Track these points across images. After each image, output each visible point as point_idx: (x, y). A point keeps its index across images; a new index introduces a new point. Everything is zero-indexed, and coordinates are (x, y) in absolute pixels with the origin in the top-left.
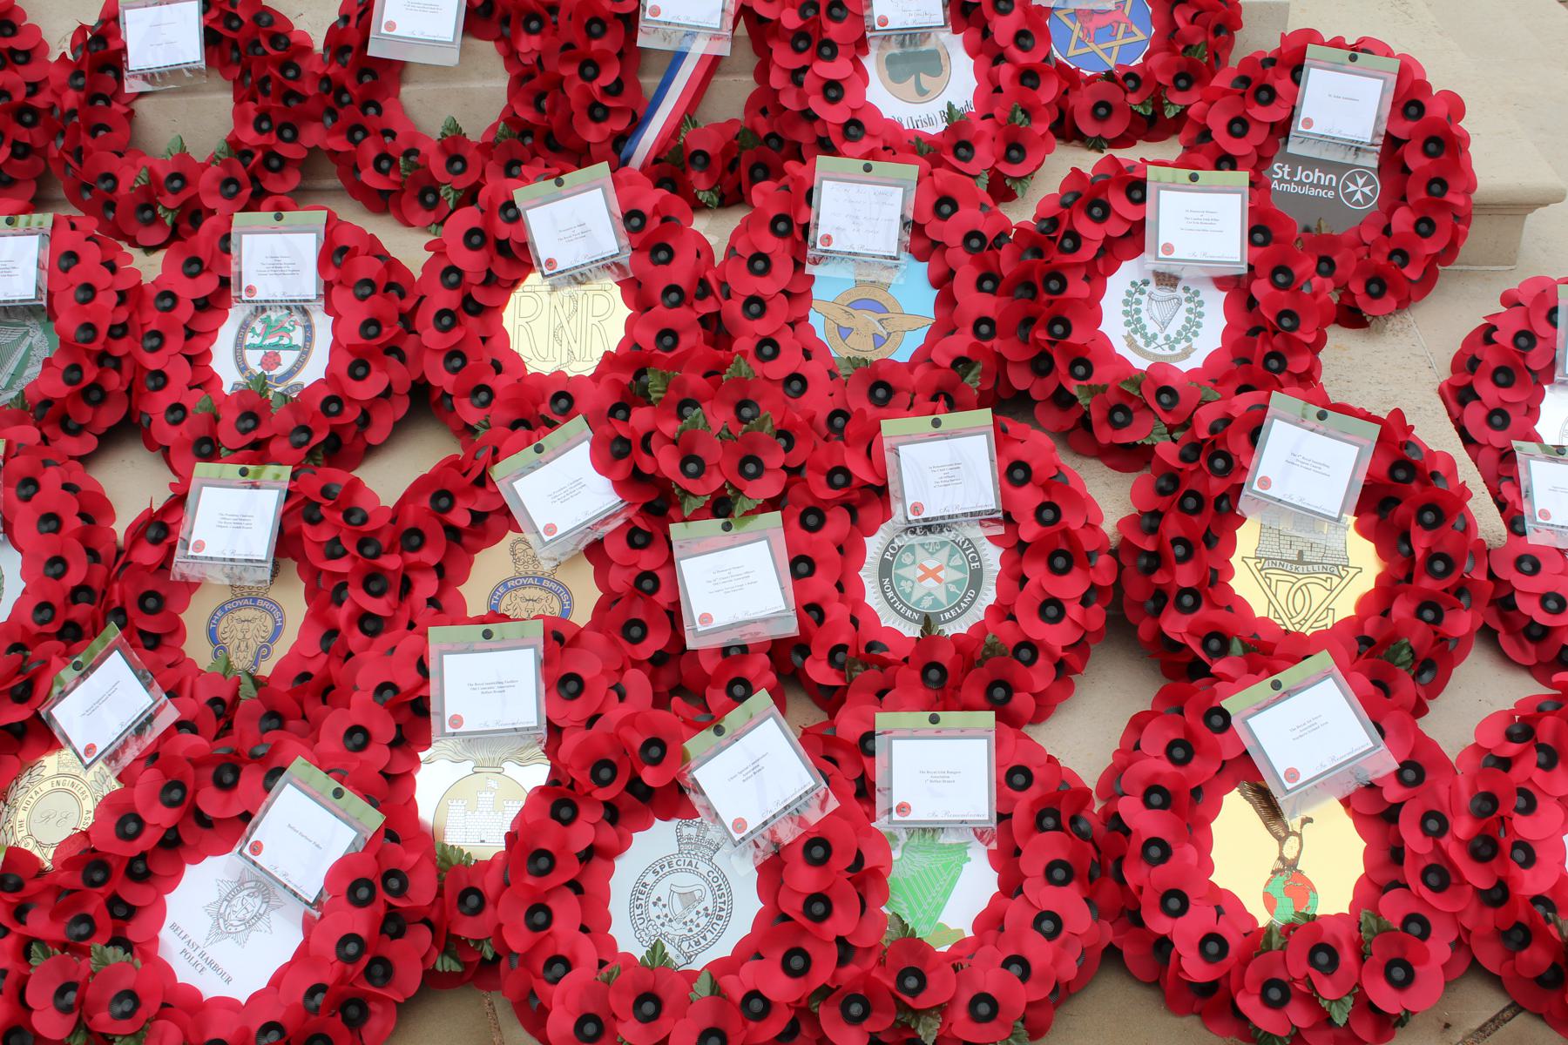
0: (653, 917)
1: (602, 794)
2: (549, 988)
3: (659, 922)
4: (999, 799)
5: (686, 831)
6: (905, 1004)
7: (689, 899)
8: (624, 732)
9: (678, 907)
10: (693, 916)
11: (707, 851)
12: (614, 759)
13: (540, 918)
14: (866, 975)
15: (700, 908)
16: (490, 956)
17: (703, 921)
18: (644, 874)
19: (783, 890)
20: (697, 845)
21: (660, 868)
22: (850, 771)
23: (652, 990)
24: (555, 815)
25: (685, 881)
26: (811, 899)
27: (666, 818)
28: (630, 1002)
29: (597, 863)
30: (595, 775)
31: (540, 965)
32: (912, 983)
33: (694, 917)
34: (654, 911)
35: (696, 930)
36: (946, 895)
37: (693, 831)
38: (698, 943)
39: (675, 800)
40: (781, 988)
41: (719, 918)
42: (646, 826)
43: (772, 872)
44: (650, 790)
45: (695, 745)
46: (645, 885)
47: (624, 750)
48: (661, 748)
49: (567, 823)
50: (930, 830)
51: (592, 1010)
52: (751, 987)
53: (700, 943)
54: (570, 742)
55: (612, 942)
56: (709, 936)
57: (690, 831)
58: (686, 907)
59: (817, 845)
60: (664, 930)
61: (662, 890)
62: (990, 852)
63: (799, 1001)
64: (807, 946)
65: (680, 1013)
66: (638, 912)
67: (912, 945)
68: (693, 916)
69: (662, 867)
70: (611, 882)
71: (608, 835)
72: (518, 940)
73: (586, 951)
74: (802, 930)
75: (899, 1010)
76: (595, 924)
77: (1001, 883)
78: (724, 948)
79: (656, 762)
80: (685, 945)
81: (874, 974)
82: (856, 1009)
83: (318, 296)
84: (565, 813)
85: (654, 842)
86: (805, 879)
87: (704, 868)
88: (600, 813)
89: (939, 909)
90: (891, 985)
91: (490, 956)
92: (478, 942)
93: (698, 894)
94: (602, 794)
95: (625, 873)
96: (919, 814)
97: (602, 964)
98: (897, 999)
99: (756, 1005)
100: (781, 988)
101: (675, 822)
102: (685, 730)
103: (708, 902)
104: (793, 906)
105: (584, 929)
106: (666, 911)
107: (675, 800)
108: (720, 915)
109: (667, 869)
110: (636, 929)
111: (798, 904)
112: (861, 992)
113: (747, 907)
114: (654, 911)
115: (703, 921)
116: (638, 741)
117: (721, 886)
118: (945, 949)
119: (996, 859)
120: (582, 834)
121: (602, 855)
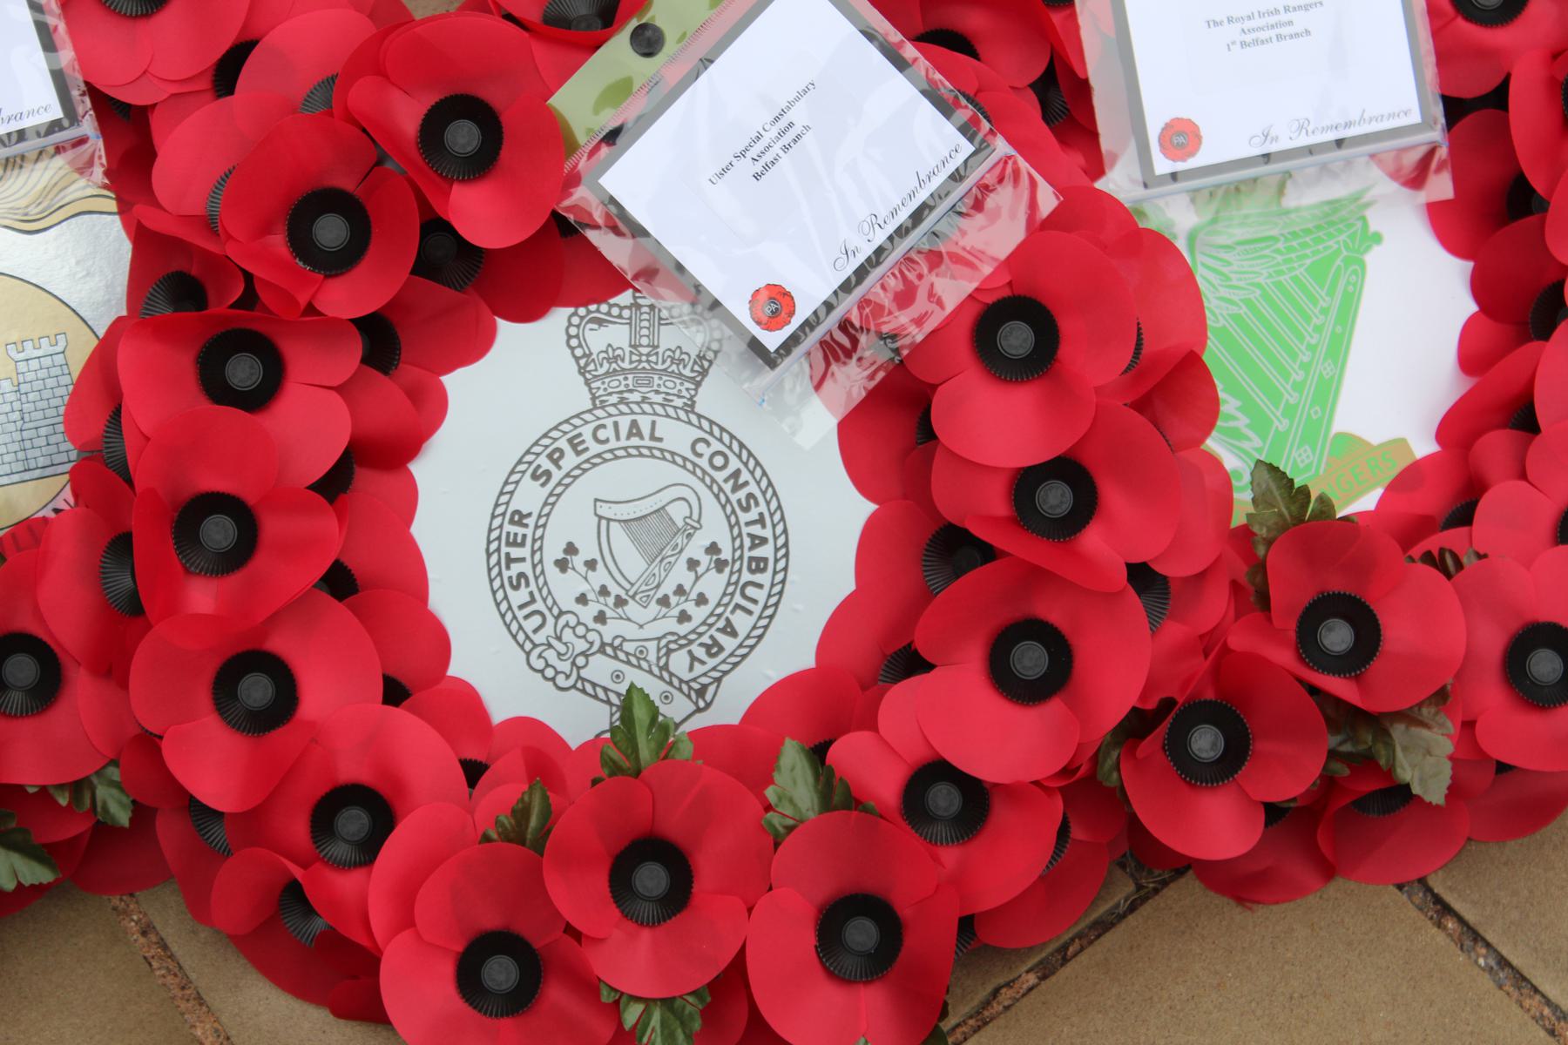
0: (568, 602)
1: (346, 298)
2: (347, 884)
3: (587, 613)
4: (1444, 57)
5: (598, 339)
6: (1338, 702)
7: (657, 531)
8: (362, 95)
9: (632, 563)
10: (680, 574)
11: (673, 385)
12: (346, 182)
13: (256, 690)
14: (1209, 642)
15: (696, 549)
16: (123, 817)
17: (713, 584)
18: (508, 488)
19: (939, 466)
20: (643, 374)
21: (550, 459)
22: (1013, 66)
23: (642, 824)
24: (218, 390)
25: (633, 481)
26: (1025, 482)
27: (528, 312)
28: (599, 882)
29: (366, 481)
30: (302, 242)
31: (298, 829)
32: (1337, 636)
33: (686, 578)
34: (565, 587)
35: (699, 614)
36: (1338, 349)
37: (616, 336)
38: (713, 648)
39: (562, 263)
40: (1007, 743)
41: (759, 565)
42: (475, 346)
43: (896, 427)
44: (468, 252)
45: (578, 101)
46: (519, 518)
47: (369, 135)
48: (487, 126)
49: (259, 399)
50: (1263, 176)
51: (490, 920)
52: (916, 754)
53: (720, 647)
54: (191, 157)
55: (468, 701)
56: (742, 623)
57: (609, 331)
58: (656, 557)
59: (1017, 324)
60: (609, 631)
61: (571, 522)
62: (1437, 214)
63: (1067, 771)
64: (1054, 612)
65: (754, 883)
66: (519, 597)
67: (1303, 521)
68: (680, 574)
69: (556, 457)
70: (418, 530)
71: (386, 399)
72: (212, 763)
73: (419, 752)
74: (1036, 576)
75: (1333, 726)
76: (412, 673)
77: (1479, 288)
78: (791, 647)
79: (481, 164)
80: (679, 662)
81: (1239, 641)
82: (1206, 742)
83: (968, 130)
84: (243, 371)
85: (512, 388)
86: (997, 428)
87: (677, 436)
88: (348, 358)
89: (1328, 392)
90: (1283, 656)
91: (123, 817)
92: (78, 787)
93: (678, 512)
94: (346, 298)
95: (451, 500)
96: (1221, 144)
97: (473, 771)
98: (1314, 690)
99: (944, 798)
100: (1007, 743)
101: (559, 317)
102: (542, 53)
103: (715, 528)
104: (982, 506)
105: (395, 693)
106: (600, 577)
107: (562, 263)
108: (759, 557)
109: (570, 460)
110: (527, 646)
111: (996, 502)
112: (1209, 695)
113: (829, 526)
114: (565, 587)
115: (713, 584)
116: (407, 114)
117: (740, 478)
118: (1368, 502)
119: (1455, 227)
120: (311, 420)
121: (380, 457)
